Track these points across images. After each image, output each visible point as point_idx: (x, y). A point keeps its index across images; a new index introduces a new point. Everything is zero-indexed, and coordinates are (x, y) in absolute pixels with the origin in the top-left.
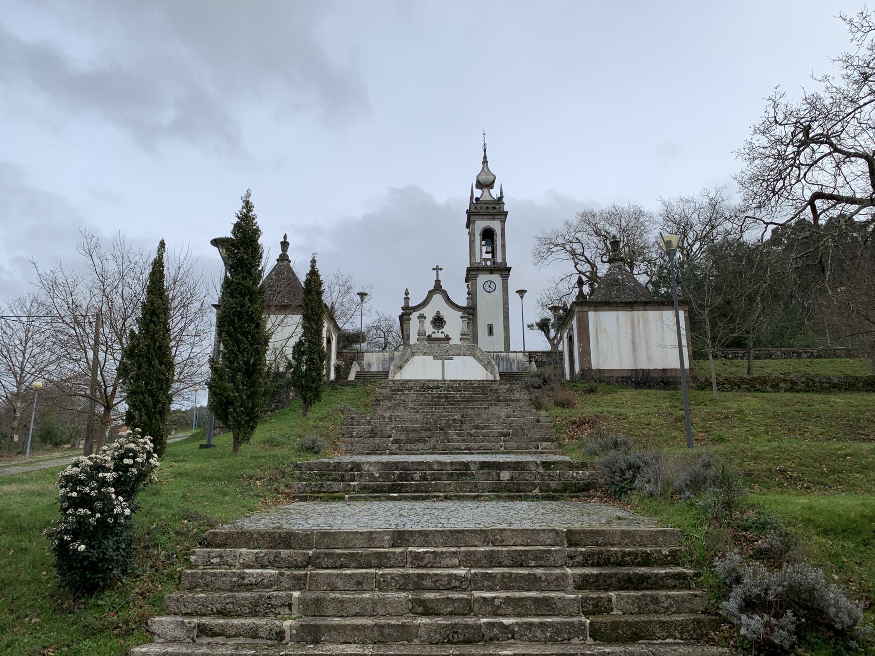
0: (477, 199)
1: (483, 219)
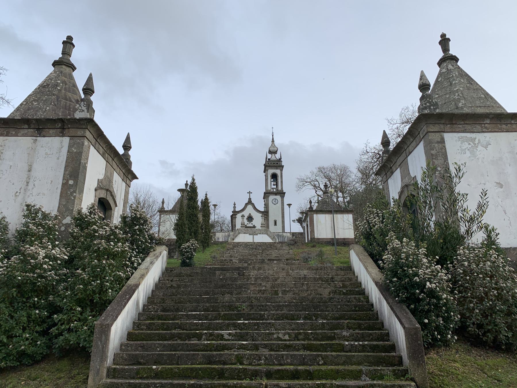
0: (269, 159)
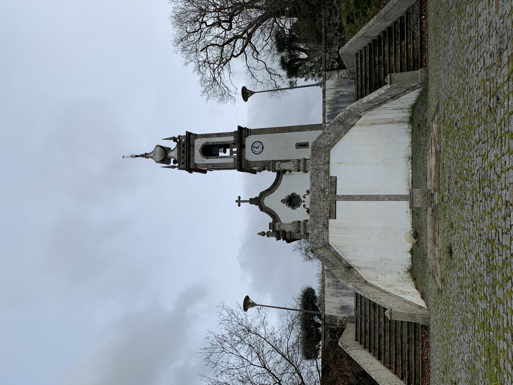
1: (193, 156)
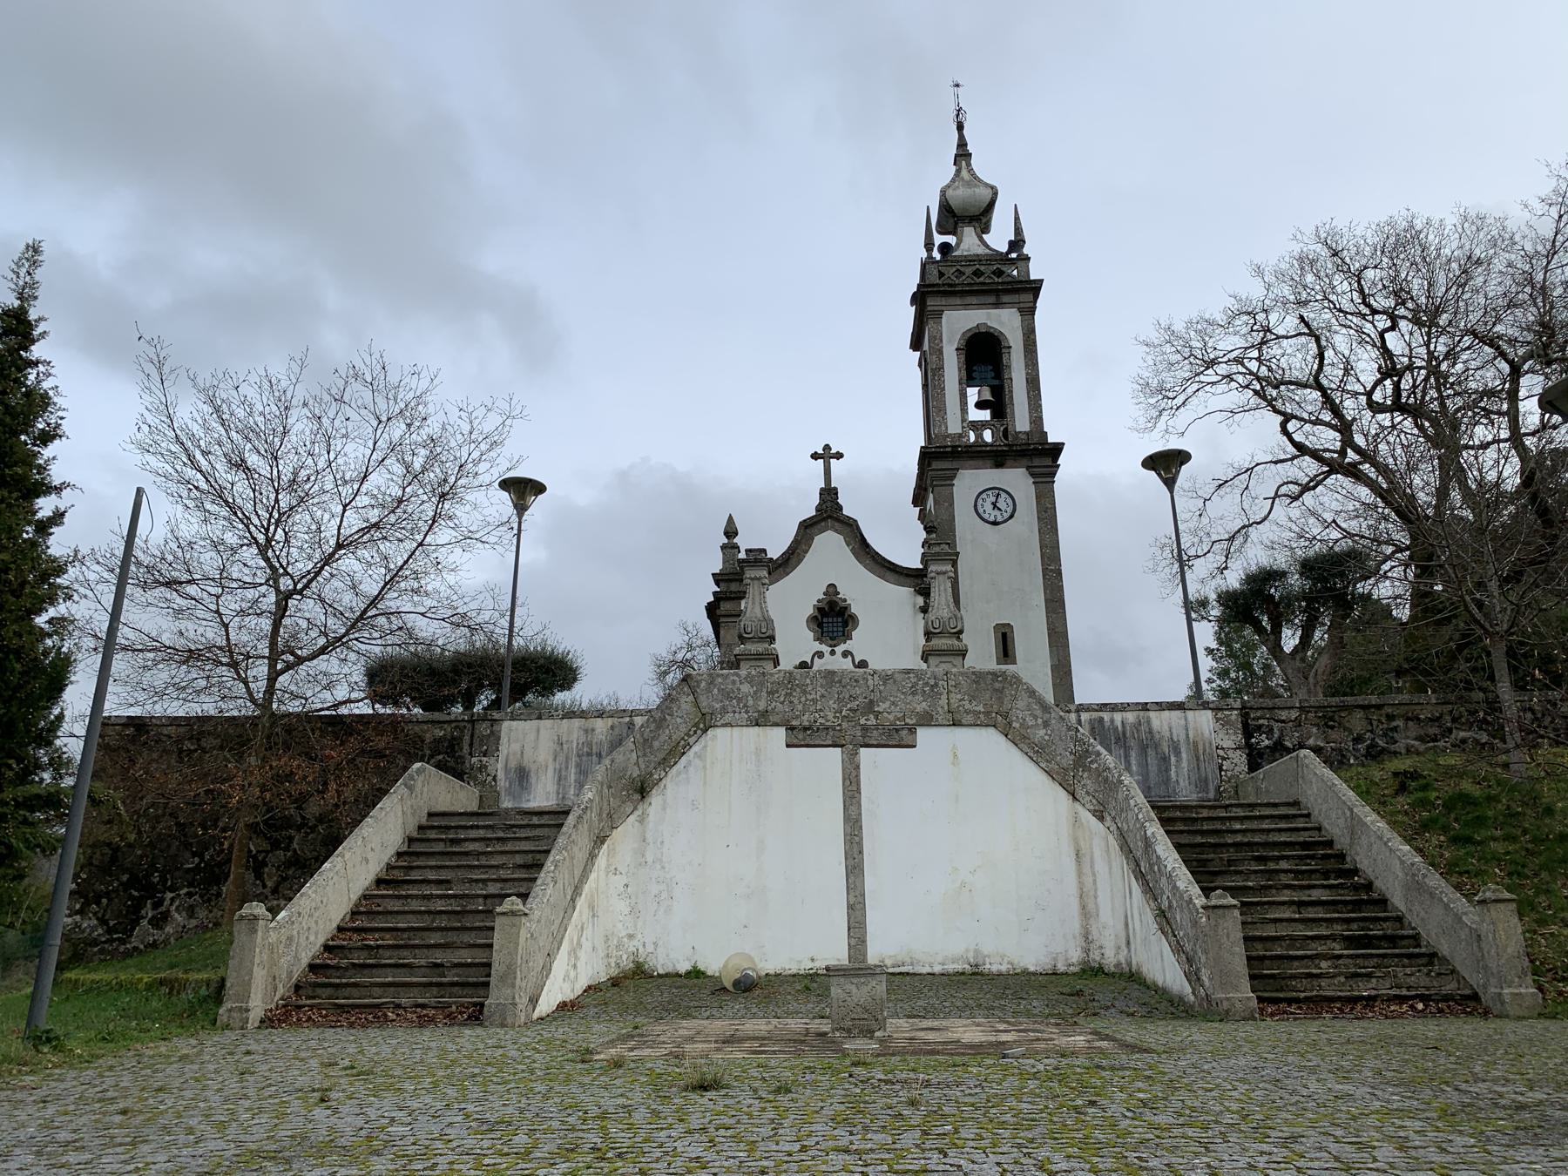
1: (966, 306)
